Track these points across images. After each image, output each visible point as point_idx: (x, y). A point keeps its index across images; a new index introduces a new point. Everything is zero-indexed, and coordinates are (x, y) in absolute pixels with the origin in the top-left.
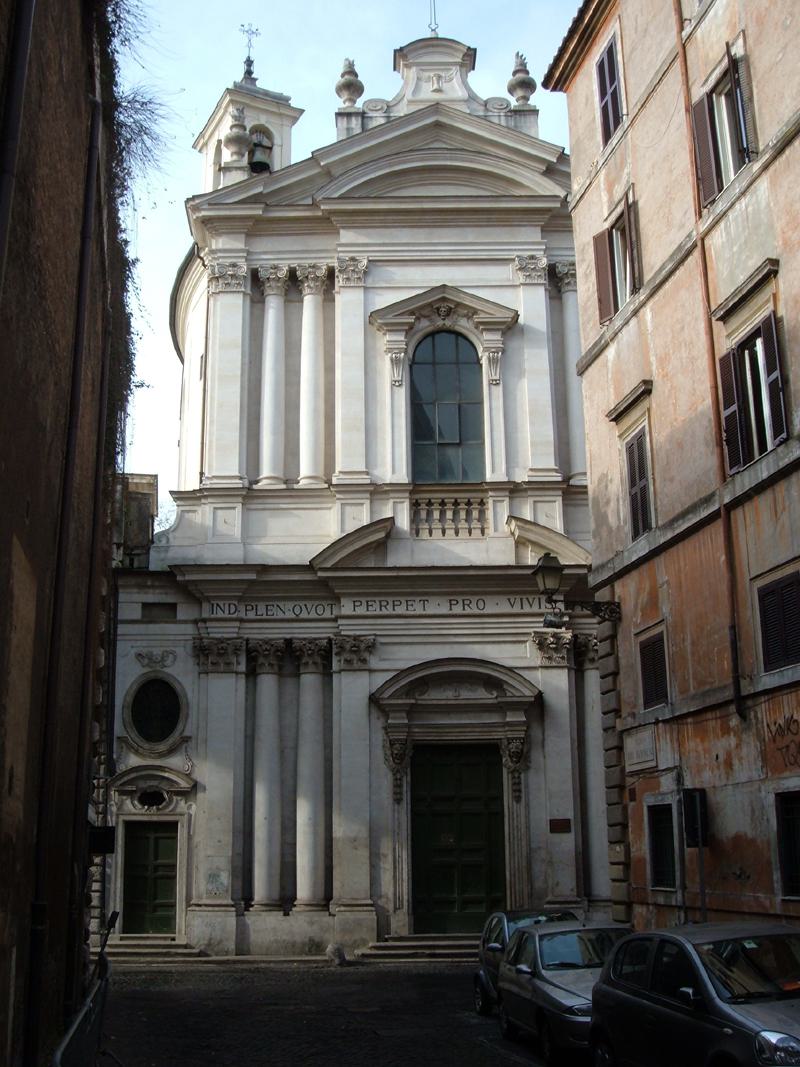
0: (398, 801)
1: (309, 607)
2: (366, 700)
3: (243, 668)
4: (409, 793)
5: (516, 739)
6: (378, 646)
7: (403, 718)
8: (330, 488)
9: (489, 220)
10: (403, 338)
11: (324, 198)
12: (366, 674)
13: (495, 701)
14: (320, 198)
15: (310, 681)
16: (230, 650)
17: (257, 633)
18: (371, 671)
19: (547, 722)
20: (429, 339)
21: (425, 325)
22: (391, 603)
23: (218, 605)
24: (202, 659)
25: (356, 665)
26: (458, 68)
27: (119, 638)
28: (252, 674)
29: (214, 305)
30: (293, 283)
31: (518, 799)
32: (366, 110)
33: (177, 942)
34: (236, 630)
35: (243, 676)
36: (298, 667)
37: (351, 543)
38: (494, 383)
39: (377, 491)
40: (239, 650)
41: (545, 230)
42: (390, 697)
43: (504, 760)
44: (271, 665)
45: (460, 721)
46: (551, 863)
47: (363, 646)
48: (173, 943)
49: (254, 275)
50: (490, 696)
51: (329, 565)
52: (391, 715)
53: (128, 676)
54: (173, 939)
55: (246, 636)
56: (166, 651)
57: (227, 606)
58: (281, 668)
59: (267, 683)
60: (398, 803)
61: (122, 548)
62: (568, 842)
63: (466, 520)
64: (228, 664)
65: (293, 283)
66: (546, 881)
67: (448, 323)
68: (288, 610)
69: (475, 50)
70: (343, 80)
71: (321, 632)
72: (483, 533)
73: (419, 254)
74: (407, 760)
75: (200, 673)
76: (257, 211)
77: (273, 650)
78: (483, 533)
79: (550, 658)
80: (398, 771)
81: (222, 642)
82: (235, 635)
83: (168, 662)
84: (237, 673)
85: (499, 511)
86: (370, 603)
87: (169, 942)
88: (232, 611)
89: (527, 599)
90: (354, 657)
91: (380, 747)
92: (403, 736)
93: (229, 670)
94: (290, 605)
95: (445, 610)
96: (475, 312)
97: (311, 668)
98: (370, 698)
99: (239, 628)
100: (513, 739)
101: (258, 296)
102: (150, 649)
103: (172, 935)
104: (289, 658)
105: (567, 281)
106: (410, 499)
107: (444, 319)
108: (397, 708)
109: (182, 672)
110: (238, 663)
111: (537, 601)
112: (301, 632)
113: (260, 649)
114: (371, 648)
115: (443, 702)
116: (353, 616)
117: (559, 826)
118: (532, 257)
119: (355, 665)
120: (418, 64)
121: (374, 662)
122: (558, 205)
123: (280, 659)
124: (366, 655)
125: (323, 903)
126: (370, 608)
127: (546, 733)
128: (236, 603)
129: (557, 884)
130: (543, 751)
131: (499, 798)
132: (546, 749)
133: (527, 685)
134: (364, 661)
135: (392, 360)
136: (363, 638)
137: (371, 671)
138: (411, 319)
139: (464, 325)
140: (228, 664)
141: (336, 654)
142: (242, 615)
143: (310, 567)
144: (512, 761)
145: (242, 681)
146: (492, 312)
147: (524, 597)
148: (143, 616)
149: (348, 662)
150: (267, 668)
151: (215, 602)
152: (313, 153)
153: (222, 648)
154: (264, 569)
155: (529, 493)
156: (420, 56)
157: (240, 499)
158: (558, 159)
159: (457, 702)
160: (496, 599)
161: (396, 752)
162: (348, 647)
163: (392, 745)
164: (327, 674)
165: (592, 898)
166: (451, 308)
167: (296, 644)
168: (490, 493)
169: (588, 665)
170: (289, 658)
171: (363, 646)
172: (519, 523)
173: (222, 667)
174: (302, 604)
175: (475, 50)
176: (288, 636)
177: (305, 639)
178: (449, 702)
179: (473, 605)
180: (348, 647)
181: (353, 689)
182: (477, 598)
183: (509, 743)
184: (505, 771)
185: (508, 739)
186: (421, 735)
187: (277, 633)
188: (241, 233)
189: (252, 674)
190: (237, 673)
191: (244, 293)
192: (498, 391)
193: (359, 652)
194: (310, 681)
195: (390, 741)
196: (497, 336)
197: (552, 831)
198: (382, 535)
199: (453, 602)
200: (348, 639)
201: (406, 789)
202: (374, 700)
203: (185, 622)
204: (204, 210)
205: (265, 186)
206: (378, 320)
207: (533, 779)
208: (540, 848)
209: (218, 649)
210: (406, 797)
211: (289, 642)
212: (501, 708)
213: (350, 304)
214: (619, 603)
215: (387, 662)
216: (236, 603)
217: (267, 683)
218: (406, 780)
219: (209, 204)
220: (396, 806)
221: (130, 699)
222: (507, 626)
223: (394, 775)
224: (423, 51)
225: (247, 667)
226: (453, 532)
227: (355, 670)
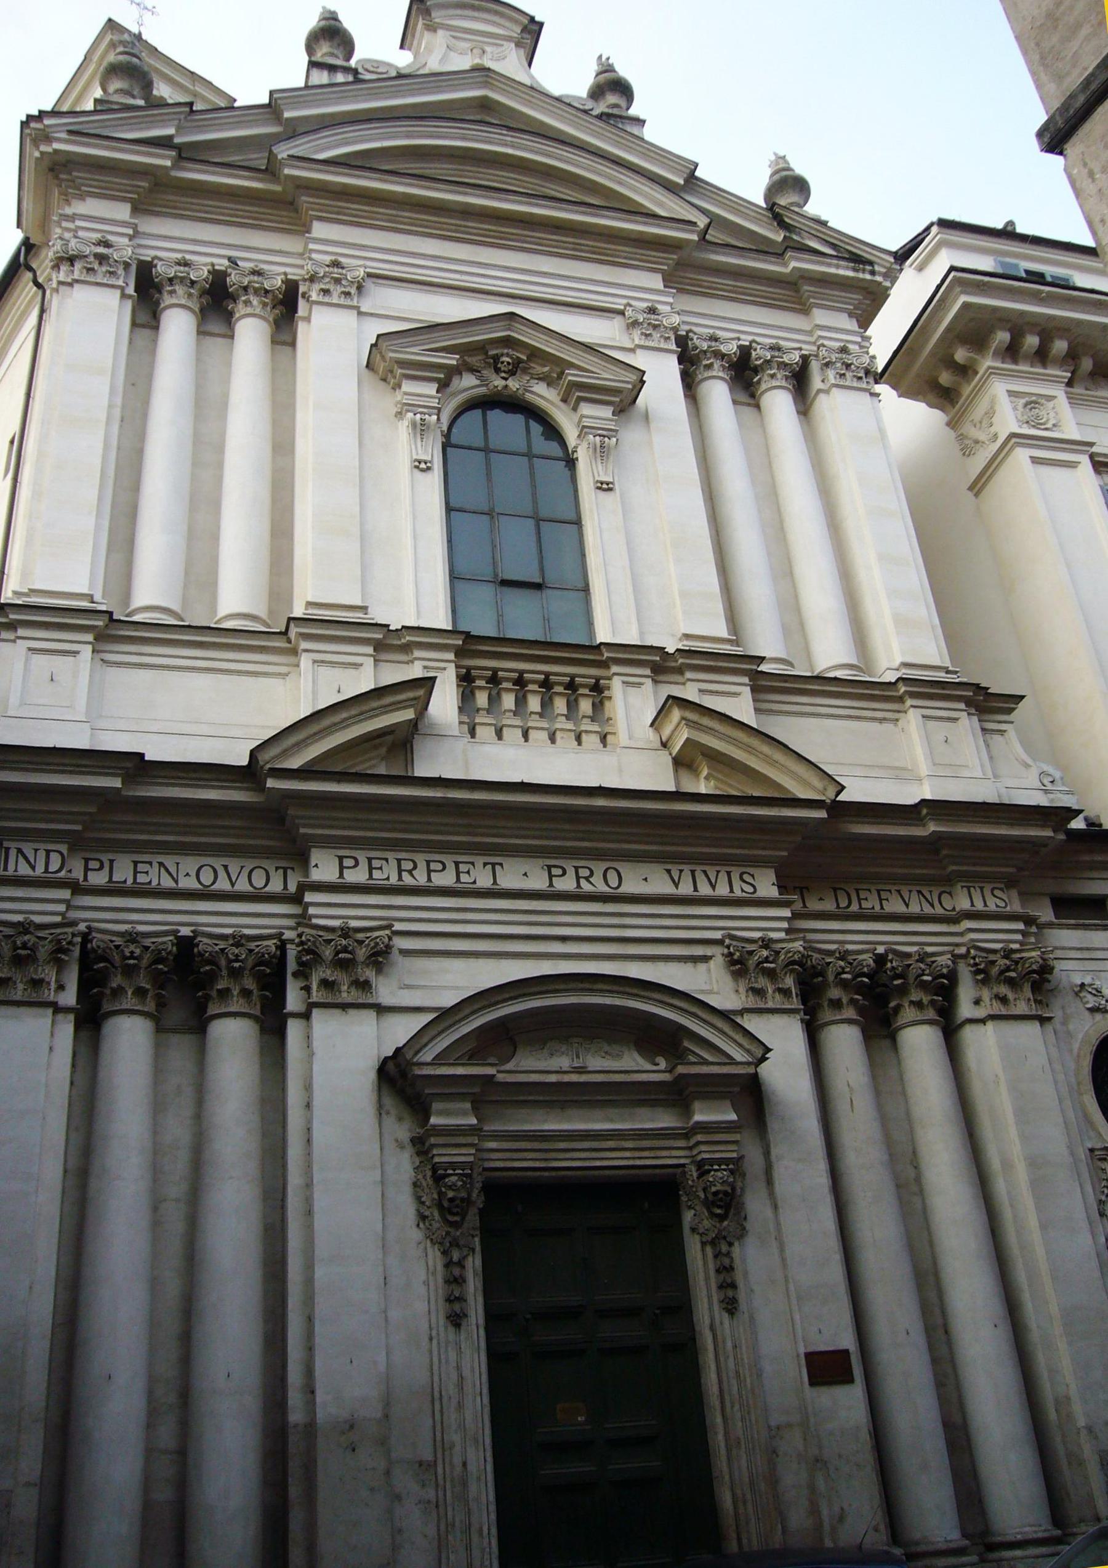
0: (456, 1320)
1: (234, 870)
2: (372, 1075)
3: (69, 997)
4: (480, 1299)
5: (720, 1161)
6: (395, 955)
7: (465, 1114)
8: (280, 637)
9: (576, 247)
10: (433, 392)
11: (291, 157)
12: (372, 1014)
13: (666, 1077)
14: (284, 155)
15: (233, 1036)
16: (43, 953)
17: (109, 917)
18: (381, 1010)
19: (773, 1125)
20: (477, 413)
23: (20, 851)
25: (346, 995)
26: (513, 45)
28: (90, 1020)
29: (59, 308)
31: (731, 1306)
32: (360, 70)
34: (62, 908)
35: (71, 1017)
36: (202, 1008)
37: (343, 725)
39: (388, 641)
40: (65, 951)
42: (440, 1059)
44: (140, 993)
45: (591, 1125)
46: (818, 1463)
47: (362, 953)
50: (649, 1067)
51: (295, 763)
52: (436, 1106)
57: (42, 855)
58: (161, 1005)
59: (130, 1038)
60: (457, 1325)
62: (847, 1403)
63: (568, 717)
64: (37, 984)
65: (217, 301)
66: (814, 1510)
67: (513, 384)
68: (187, 872)
69: (541, 25)
70: (323, 23)
71: (263, 921)
72: (604, 739)
73: (457, 276)
74: (473, 1218)
76: (163, 160)
78: (604, 739)
79: (759, 992)
80: (455, 1244)
81: (27, 932)
82: (58, 919)
84: (57, 1009)
85: (633, 704)
86: (376, 863)
89: (705, 872)
90: (342, 978)
91: (408, 1189)
92: (464, 1155)
93: (36, 1001)
94: (189, 864)
95: (538, 882)
96: (562, 365)
97: (236, 1004)
98: (383, 1071)
99: (69, 907)
100: (712, 1162)
101: (143, 318)
104: (186, 983)
105: (705, 362)
106: (457, 667)
107: (506, 379)
108: (453, 1089)
110: (61, 987)
111: (723, 877)
112: (217, 920)
113: (117, 958)
114: (380, 957)
115: (553, 1078)
116: (341, 890)
117: (827, 1368)
119: (344, 995)
120: (448, 28)
121: (386, 992)
122: (695, 237)
123: (160, 981)
124: (369, 974)
126: (376, 874)
127: (774, 1152)
128: (65, 852)
129: (841, 1518)
130: (771, 1194)
131: (681, 1308)
132: (779, 1188)
133: (738, 1037)
134: (365, 986)
135: (414, 424)
136: (360, 936)
137: (381, 1010)
140: (37, 984)
141: (295, 975)
142: (78, 874)
143: (250, 773)
144: (713, 1215)
145: (67, 1028)
146: (594, 370)
149: (327, 985)
150: (129, 1001)
151: (13, 845)
152: (271, 93)
153: (24, 946)
154: (134, 765)
155: (689, 675)
156: (452, 17)
157: (90, 637)
158: (686, 181)
159: (583, 1078)
160: (645, 869)
161: (451, 1194)
162: (328, 953)
163: (438, 1179)
164: (272, 1025)
166: (519, 361)
168: (615, 669)
169: (827, 1015)
170: (186, 983)
171: (362, 953)
172: (689, 715)
173: (19, 992)
174: (217, 862)
175: (541, 25)
176: (185, 931)
177: (224, 937)
178: (567, 1078)
179: (597, 879)
180: (328, 953)
181: (341, 1052)
182: (604, 865)
183: (702, 1174)
186: (503, 1158)
187: (156, 919)
188: (123, 200)
189: (90, 1020)
190: (57, 1009)
191: (124, 296)
193: (351, 967)
194: (233, 1036)
195: (434, 1169)
196: (606, 412)
197: (813, 1383)
199: (555, 871)
200: (328, 936)
201: (473, 1286)
202: (396, 1076)
204: (59, 140)
205: (179, 128)
206: (386, 362)
207: (753, 1259)
208: (789, 1425)
209: (16, 948)
211: (186, 945)
212: (678, 1094)
213: (332, 339)
215: (418, 993)
216: (64, 849)
217: (130, 1038)
218: (474, 1264)
219: (70, 132)
220: (451, 1329)
222: (668, 923)
223: (445, 1253)
224: (459, 12)
225: (78, 1002)
227: (344, 1007)
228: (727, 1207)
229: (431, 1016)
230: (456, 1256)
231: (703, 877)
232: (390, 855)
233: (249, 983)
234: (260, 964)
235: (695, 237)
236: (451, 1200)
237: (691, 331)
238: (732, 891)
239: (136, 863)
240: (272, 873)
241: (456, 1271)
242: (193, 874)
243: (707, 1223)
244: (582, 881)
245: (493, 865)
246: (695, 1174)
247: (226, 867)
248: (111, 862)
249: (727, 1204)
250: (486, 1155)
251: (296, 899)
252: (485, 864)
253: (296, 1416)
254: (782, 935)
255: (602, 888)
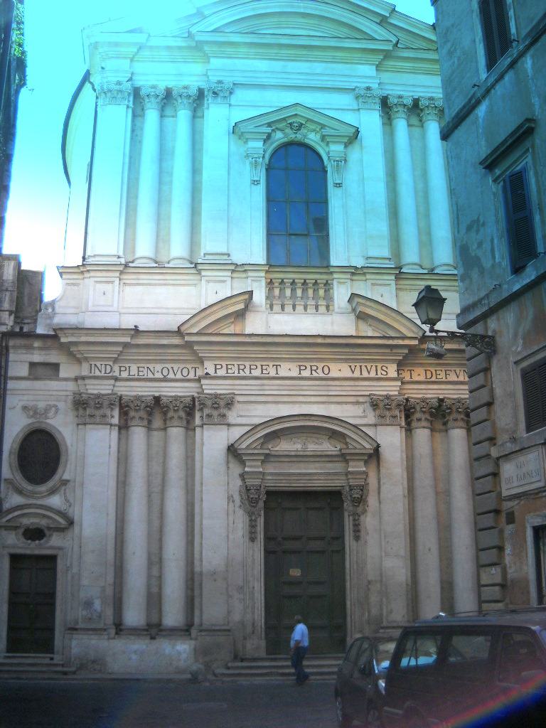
0: (252, 540)
3: (116, 420)
21: (279, 137)
22: (248, 367)
24: (81, 411)
27: (8, 392)
28: (124, 427)
30: (168, 97)
31: (357, 538)
33: (55, 662)
34: (111, 387)
38: (339, 185)
41: (378, 67)
43: (345, 504)
48: (52, 662)
49: (136, 92)
53: (16, 425)
54: (52, 659)
55: (119, 393)
56: (50, 405)
57: (103, 366)
61: (13, 315)
74: (261, 504)
75: (78, 425)
77: (143, 405)
83: (51, 414)
87: (47, 661)
88: (108, 371)
89: (366, 366)
92: (257, 482)
93: (104, 421)
102: (35, 403)
103: (51, 656)
109: (63, 425)
118: (368, 89)
125: (186, 628)
131: (340, 538)
138: (269, 130)
139: (313, 138)
145: (115, 433)
147: (363, 365)
148: (30, 374)
161: (252, 496)
165: (122, 627)
167: (164, 400)
183: (351, 490)
184: (346, 514)
185: (350, 486)
189: (124, 427)
190: (111, 425)
192: (338, 191)
198: (242, 306)
203: (66, 379)
210: (261, 536)
211: (157, 400)
213: (217, 117)
214: (494, 337)
217: (138, 435)
221: (16, 446)
223: (250, 516)
226: (302, 308)
228: (359, 503)
229: (249, 428)
230: (253, 518)
231: (365, 368)
232: (235, 363)
233: (182, 414)
234: (147, 407)
235: (391, 48)
236: (252, 498)
237: (389, 95)
238: (377, 374)
239: (138, 367)
240: (190, 369)
241: (253, 523)
242: (160, 371)
243: (351, 508)
244: (313, 372)
245: (277, 365)
246: (348, 490)
247: (172, 368)
248: (129, 367)
249: (360, 501)
250: (266, 481)
251: (199, 380)
252: (273, 365)
253: (197, 569)
254: (397, 393)
255: (322, 375)
